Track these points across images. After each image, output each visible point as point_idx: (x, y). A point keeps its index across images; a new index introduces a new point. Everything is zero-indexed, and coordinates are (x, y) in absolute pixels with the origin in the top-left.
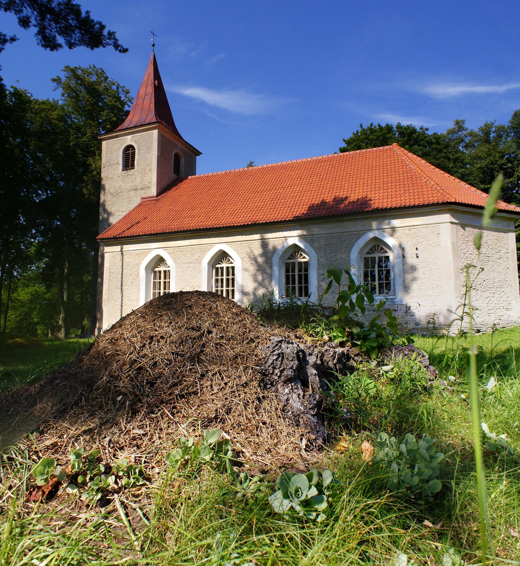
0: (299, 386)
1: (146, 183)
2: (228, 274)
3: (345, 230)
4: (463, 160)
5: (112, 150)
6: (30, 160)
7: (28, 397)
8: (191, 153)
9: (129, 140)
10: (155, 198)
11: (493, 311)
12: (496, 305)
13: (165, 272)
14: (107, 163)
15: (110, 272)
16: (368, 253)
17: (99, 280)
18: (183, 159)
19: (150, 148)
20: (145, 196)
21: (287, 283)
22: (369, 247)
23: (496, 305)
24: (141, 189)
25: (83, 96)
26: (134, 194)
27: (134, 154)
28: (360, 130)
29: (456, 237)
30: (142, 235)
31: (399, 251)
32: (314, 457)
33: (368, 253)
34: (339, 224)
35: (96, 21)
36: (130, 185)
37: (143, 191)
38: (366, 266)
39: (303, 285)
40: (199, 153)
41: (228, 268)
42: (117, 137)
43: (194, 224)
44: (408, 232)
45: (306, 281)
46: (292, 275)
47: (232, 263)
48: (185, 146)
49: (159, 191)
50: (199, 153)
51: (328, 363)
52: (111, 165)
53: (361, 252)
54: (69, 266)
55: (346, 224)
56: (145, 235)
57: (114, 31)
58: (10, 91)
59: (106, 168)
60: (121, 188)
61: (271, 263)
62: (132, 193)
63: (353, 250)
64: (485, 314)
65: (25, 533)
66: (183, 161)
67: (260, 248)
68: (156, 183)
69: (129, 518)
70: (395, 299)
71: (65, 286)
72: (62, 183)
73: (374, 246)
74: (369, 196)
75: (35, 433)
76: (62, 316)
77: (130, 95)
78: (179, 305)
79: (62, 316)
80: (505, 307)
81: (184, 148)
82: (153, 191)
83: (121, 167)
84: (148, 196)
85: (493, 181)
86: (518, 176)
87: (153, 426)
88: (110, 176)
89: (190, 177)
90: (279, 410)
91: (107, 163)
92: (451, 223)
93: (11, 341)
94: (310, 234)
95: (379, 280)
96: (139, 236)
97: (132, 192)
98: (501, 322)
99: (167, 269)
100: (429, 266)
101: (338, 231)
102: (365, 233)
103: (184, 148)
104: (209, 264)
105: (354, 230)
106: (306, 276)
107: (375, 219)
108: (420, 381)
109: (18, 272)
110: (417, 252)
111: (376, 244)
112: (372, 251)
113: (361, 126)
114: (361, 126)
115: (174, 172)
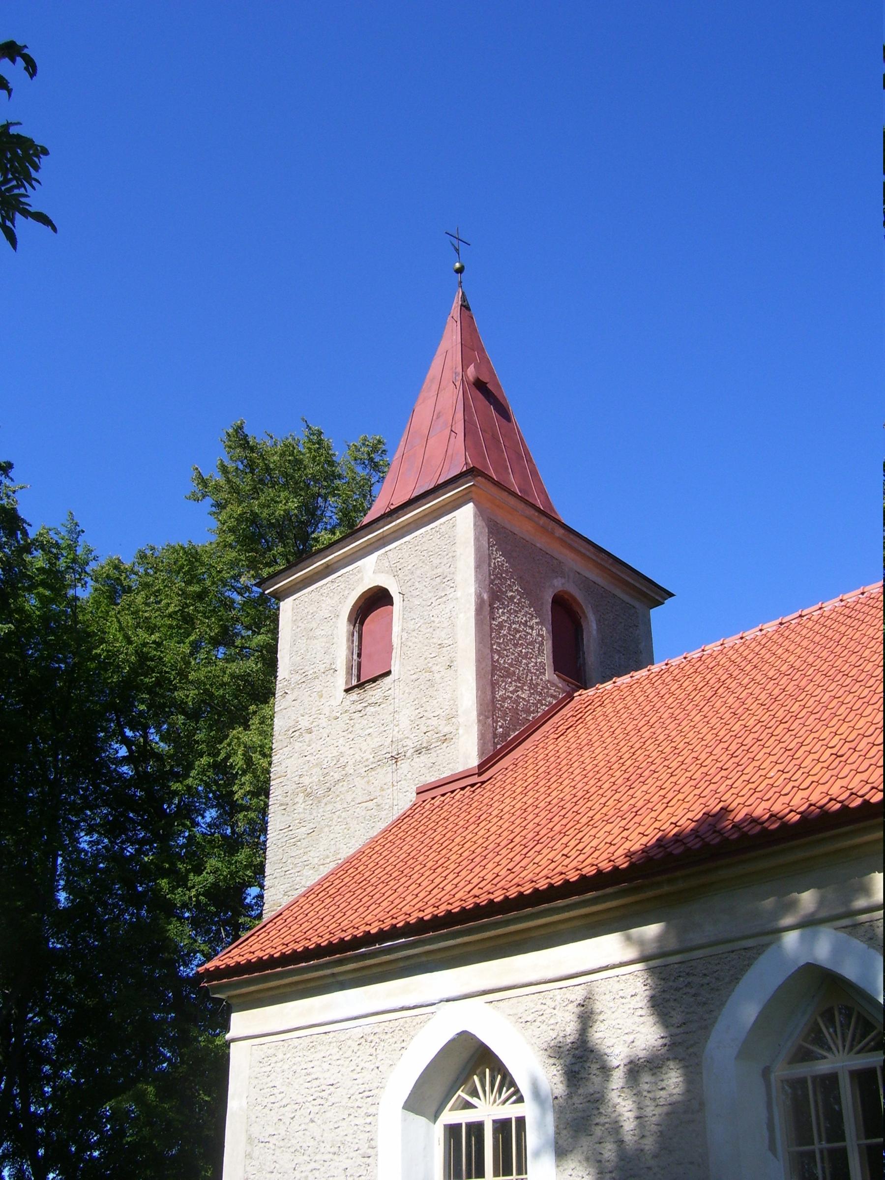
0: (181, 841)
1: (434, 722)
5: (311, 624)
8: (626, 598)
9: (368, 572)
10: (475, 779)
14: (297, 677)
15: (250, 1140)
16: (804, 1056)
19: (445, 580)
20: (431, 778)
24: (418, 752)
26: (389, 779)
28: (36, 199)
29: (489, 668)
35: (32, 534)
36: (375, 742)
37: (423, 758)
40: (656, 595)
42: (328, 570)
43: (355, 1014)
48: (598, 565)
50: (656, 595)
52: (306, 680)
56: (394, 932)
59: (290, 697)
60: (343, 760)
62: (384, 775)
66: (591, 626)
67: (650, 1020)
68: (790, 973)
76: (151, 1097)
79: (151, 1097)
81: (593, 575)
82: (466, 753)
84: (446, 773)
85: (785, 826)
86: (826, 993)
88: (304, 723)
89: (576, 694)
91: (297, 677)
92: (30, 525)
95: (844, 1151)
99: (510, 1111)
103: (593, 575)
104: (349, 620)
107: (800, 875)
108: (145, 729)
113: (42, 218)
114: (42, 218)
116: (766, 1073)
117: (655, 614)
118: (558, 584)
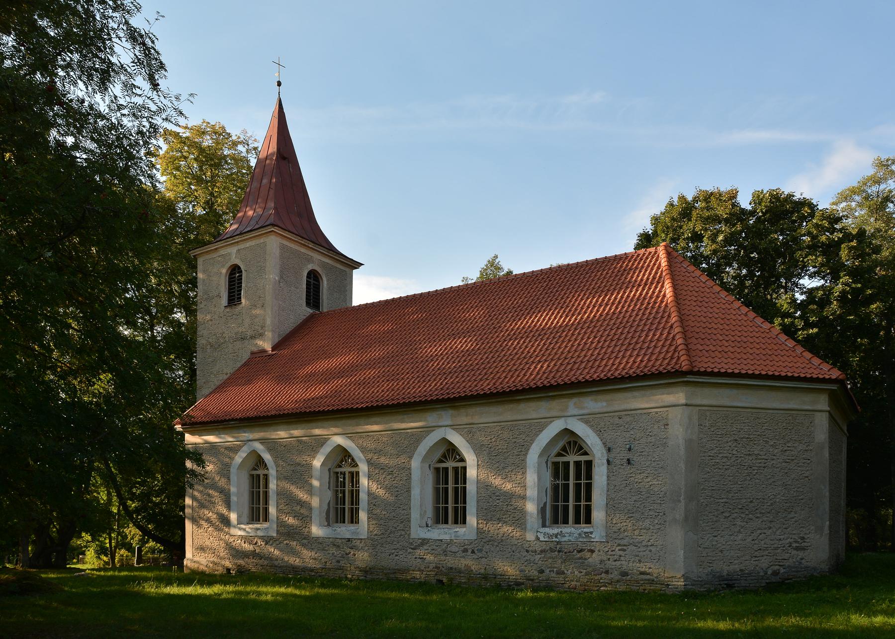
2: (578, 476)
3: (519, 417)
4: (673, 219)
9: (232, 254)
11: (766, 553)
12: (772, 542)
13: (456, 469)
16: (559, 455)
17: (224, 596)
18: (324, 279)
21: (252, 501)
22: (561, 444)
23: (772, 542)
30: (229, 420)
31: (602, 453)
33: (559, 455)
34: (511, 406)
38: (556, 475)
39: (583, 503)
40: (357, 265)
41: (578, 464)
42: (329, 483)
44: (617, 420)
47: (586, 453)
49: (277, 341)
50: (357, 265)
53: (544, 452)
55: (522, 406)
56: (233, 420)
62: (238, 344)
63: (531, 451)
64: (747, 557)
65: (221, 458)
66: (325, 283)
70: (591, 533)
72: (867, 424)
73: (569, 443)
78: (706, 246)
80: (794, 545)
81: (261, 562)
83: (224, 301)
90: (443, 558)
94: (689, 402)
96: (225, 420)
97: (238, 343)
98: (782, 571)
100: (649, 480)
101: (509, 418)
102: (551, 422)
105: (534, 416)
106: (589, 487)
109: (180, 376)
110: (630, 456)
111: (572, 439)
112: (443, 458)
115: (308, 304)
116: (329, 470)
117: (354, 271)
118: (310, 267)
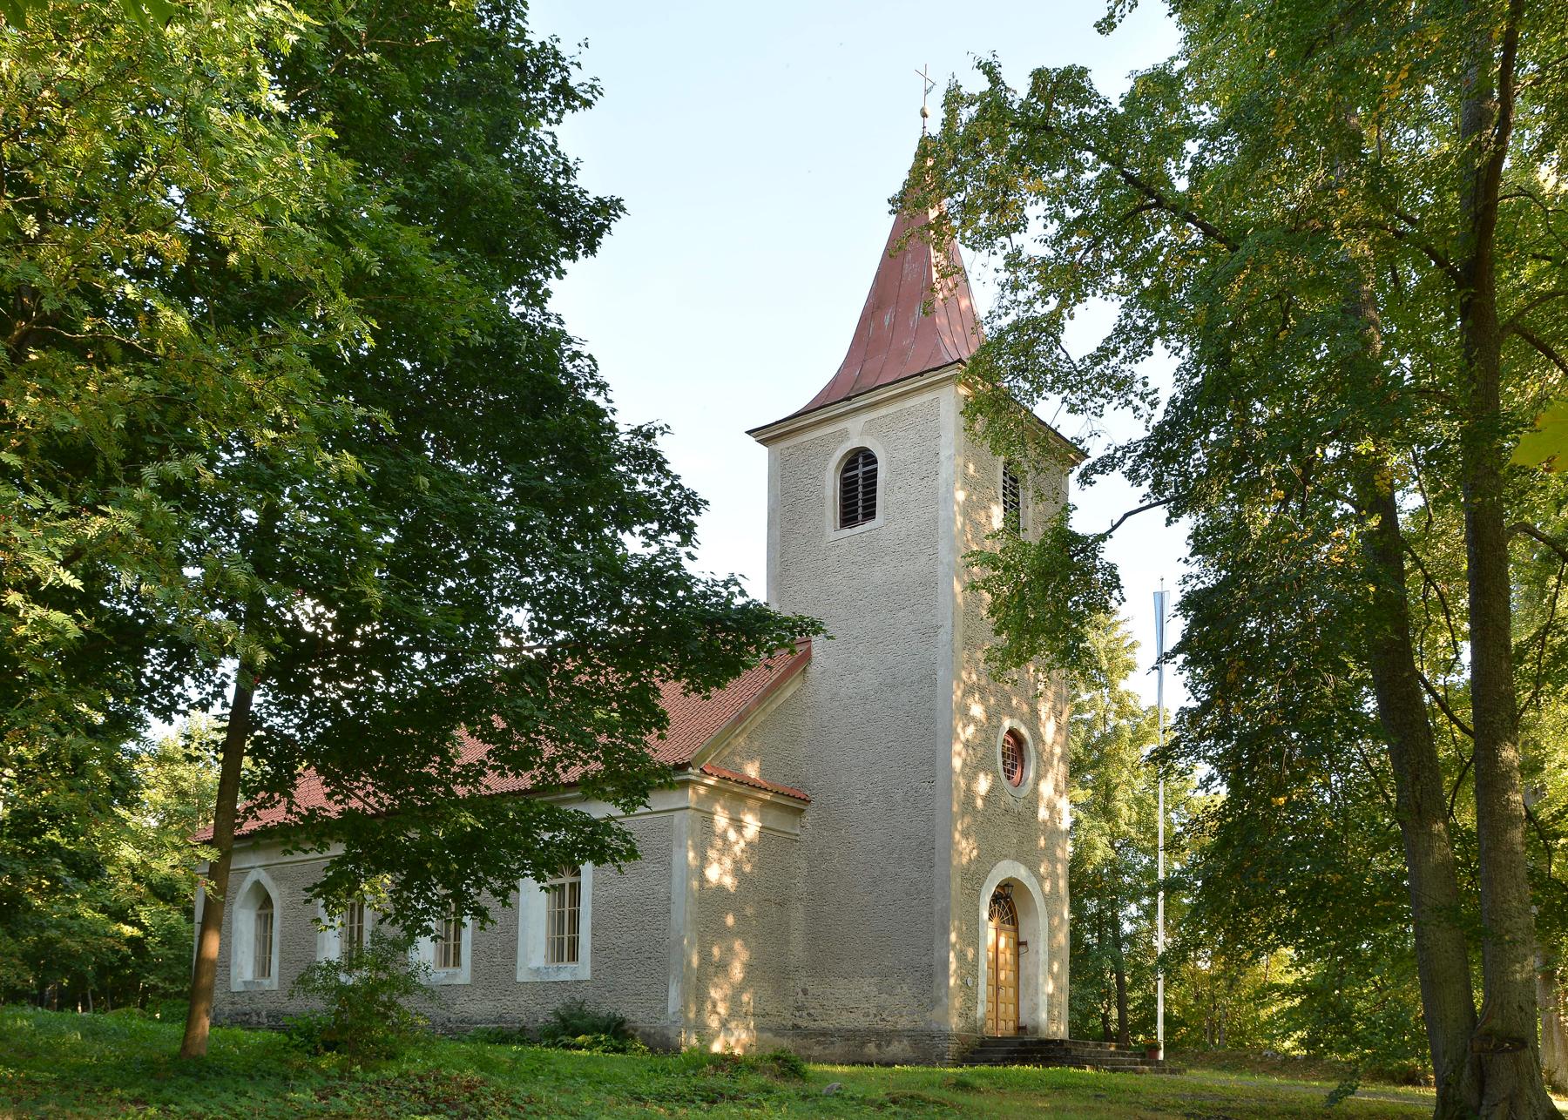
6: (277, 607)
7: (639, 585)
25: (1323, 696)
27: (871, 477)
32: (1083, 992)
45: (360, 920)
46: (573, 885)
50: (1083, 72)
51: (644, 803)
54: (1295, 1058)
57: (605, 194)
58: (1376, 310)
61: (966, 796)
69: (574, 880)
71: (1476, 969)
74: (578, 997)
75: (982, 776)
77: (1066, 407)
87: (1055, 799)
93: (84, 708)
